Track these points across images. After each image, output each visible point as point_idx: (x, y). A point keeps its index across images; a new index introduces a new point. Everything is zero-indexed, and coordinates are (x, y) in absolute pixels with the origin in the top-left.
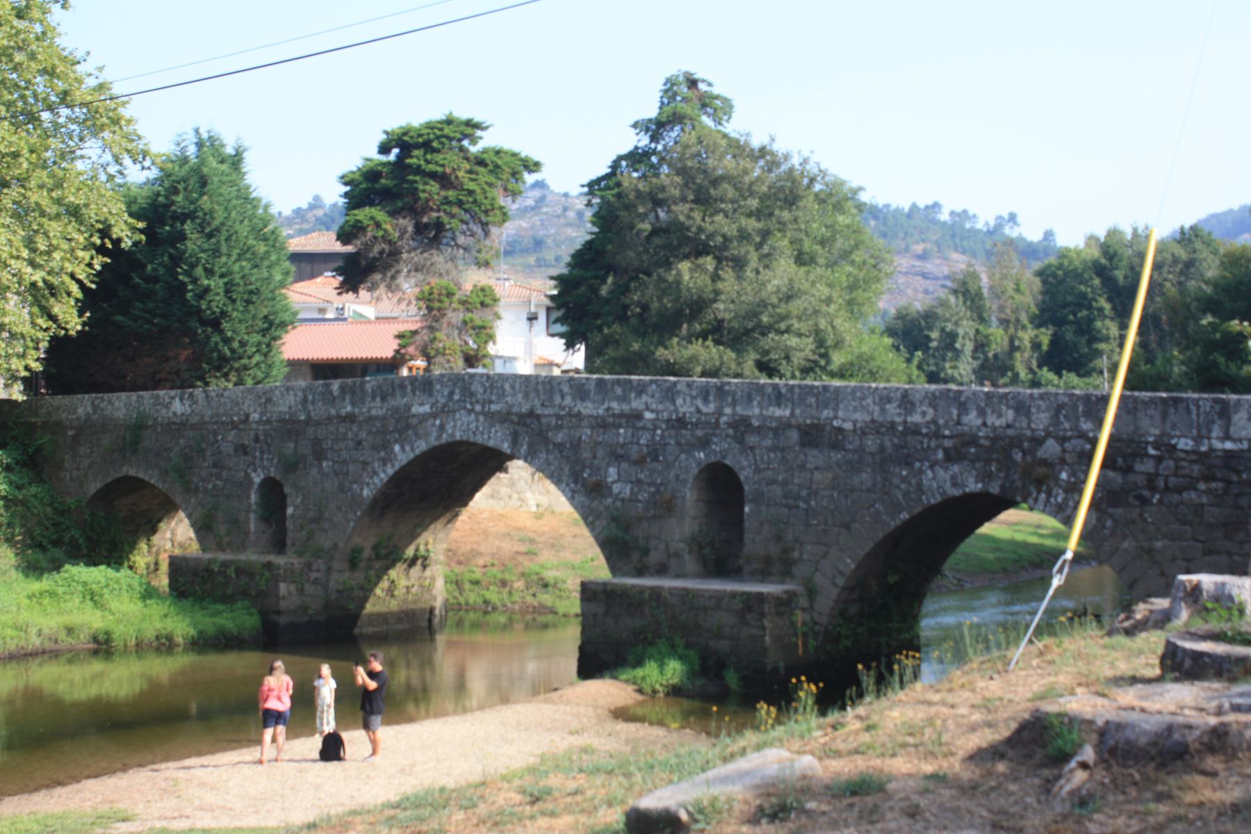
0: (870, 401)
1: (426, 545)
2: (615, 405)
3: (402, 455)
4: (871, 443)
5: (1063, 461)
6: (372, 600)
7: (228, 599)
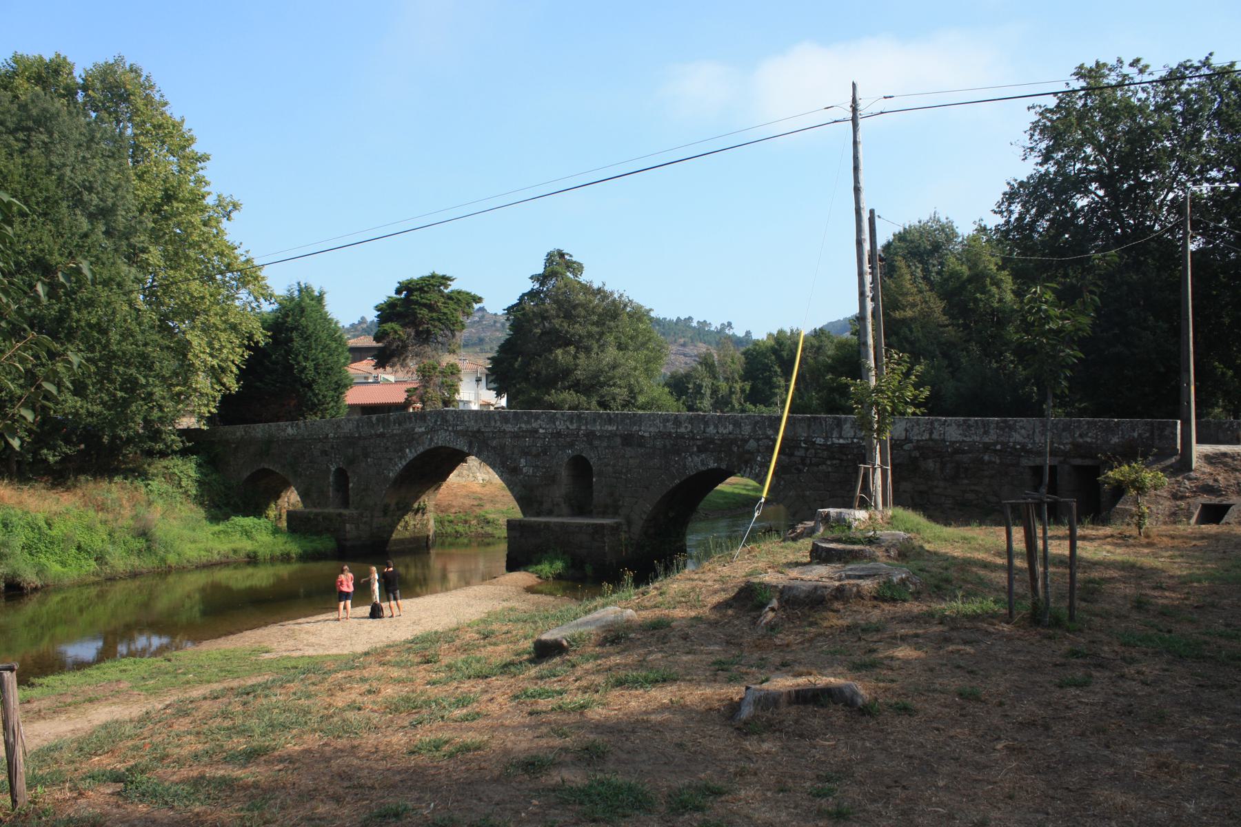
2: (523, 426)
3: (410, 454)
4: (659, 443)
6: (395, 532)
7: (319, 533)
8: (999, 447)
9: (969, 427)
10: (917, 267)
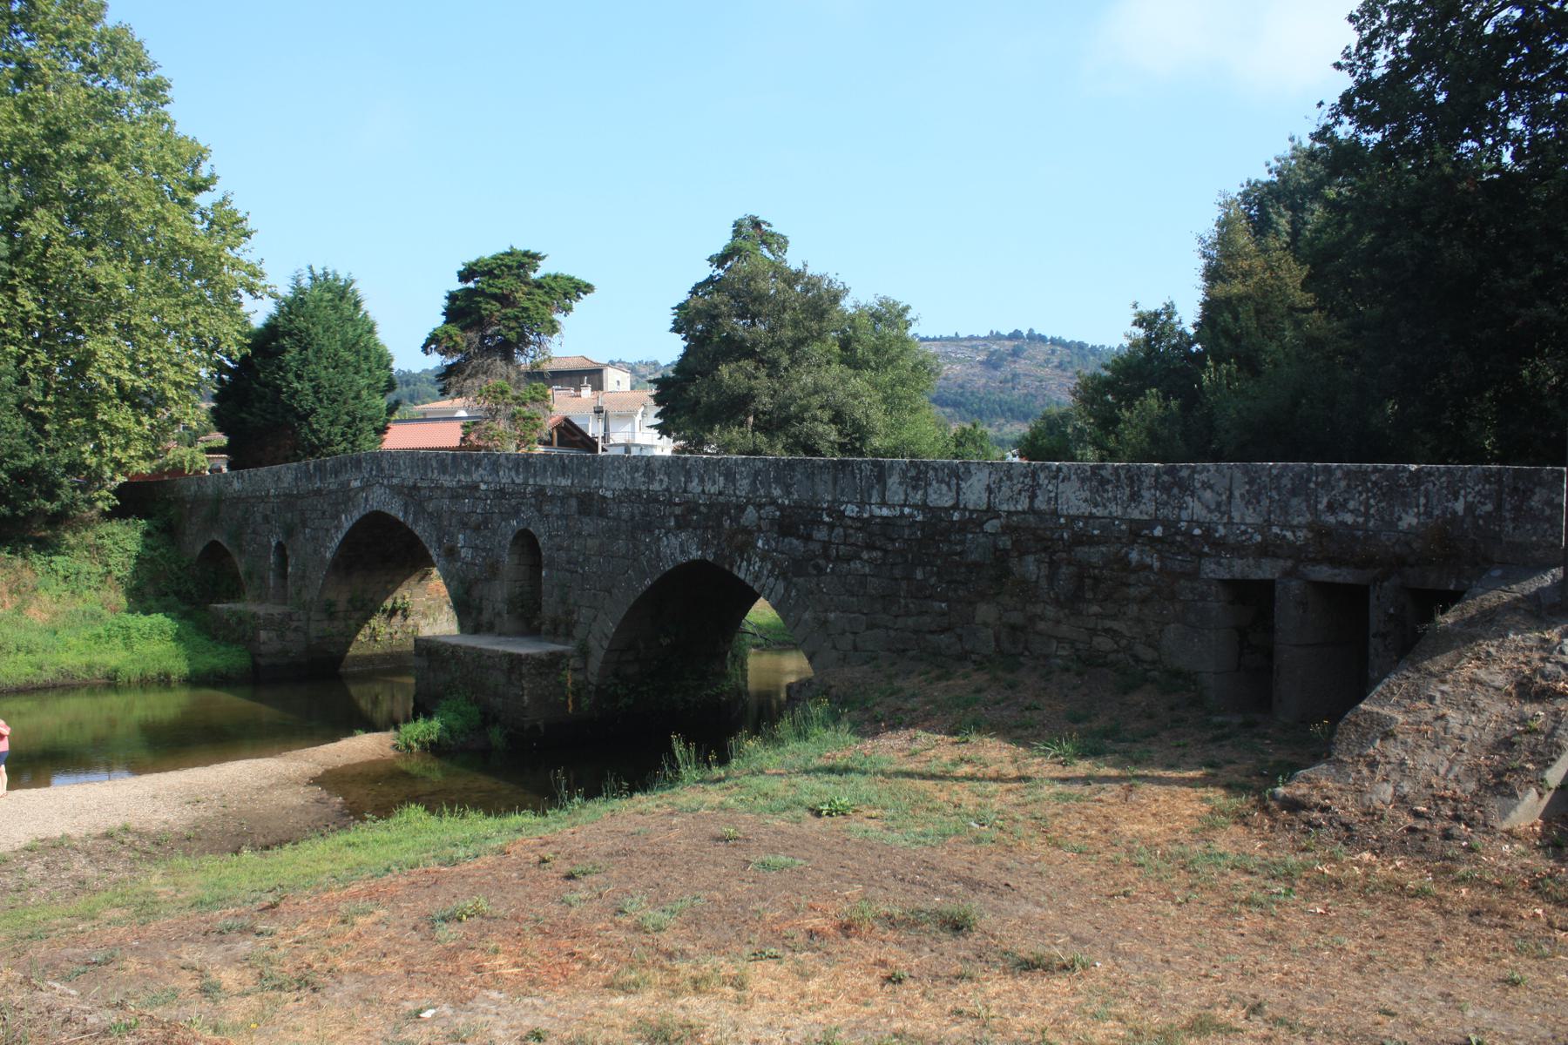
0: (624, 470)
1: (404, 598)
2: (462, 477)
3: (347, 522)
5: (760, 529)
6: (354, 645)
8: (1158, 532)
9: (1104, 482)
10: (1281, 216)
